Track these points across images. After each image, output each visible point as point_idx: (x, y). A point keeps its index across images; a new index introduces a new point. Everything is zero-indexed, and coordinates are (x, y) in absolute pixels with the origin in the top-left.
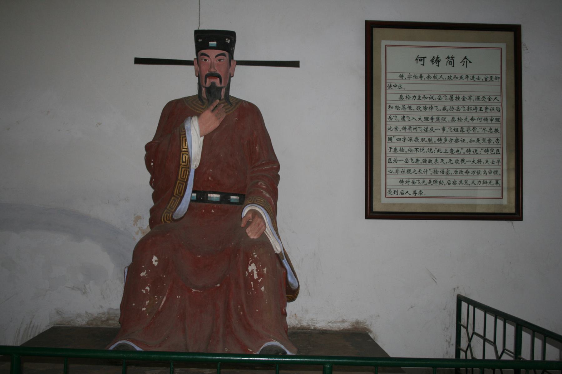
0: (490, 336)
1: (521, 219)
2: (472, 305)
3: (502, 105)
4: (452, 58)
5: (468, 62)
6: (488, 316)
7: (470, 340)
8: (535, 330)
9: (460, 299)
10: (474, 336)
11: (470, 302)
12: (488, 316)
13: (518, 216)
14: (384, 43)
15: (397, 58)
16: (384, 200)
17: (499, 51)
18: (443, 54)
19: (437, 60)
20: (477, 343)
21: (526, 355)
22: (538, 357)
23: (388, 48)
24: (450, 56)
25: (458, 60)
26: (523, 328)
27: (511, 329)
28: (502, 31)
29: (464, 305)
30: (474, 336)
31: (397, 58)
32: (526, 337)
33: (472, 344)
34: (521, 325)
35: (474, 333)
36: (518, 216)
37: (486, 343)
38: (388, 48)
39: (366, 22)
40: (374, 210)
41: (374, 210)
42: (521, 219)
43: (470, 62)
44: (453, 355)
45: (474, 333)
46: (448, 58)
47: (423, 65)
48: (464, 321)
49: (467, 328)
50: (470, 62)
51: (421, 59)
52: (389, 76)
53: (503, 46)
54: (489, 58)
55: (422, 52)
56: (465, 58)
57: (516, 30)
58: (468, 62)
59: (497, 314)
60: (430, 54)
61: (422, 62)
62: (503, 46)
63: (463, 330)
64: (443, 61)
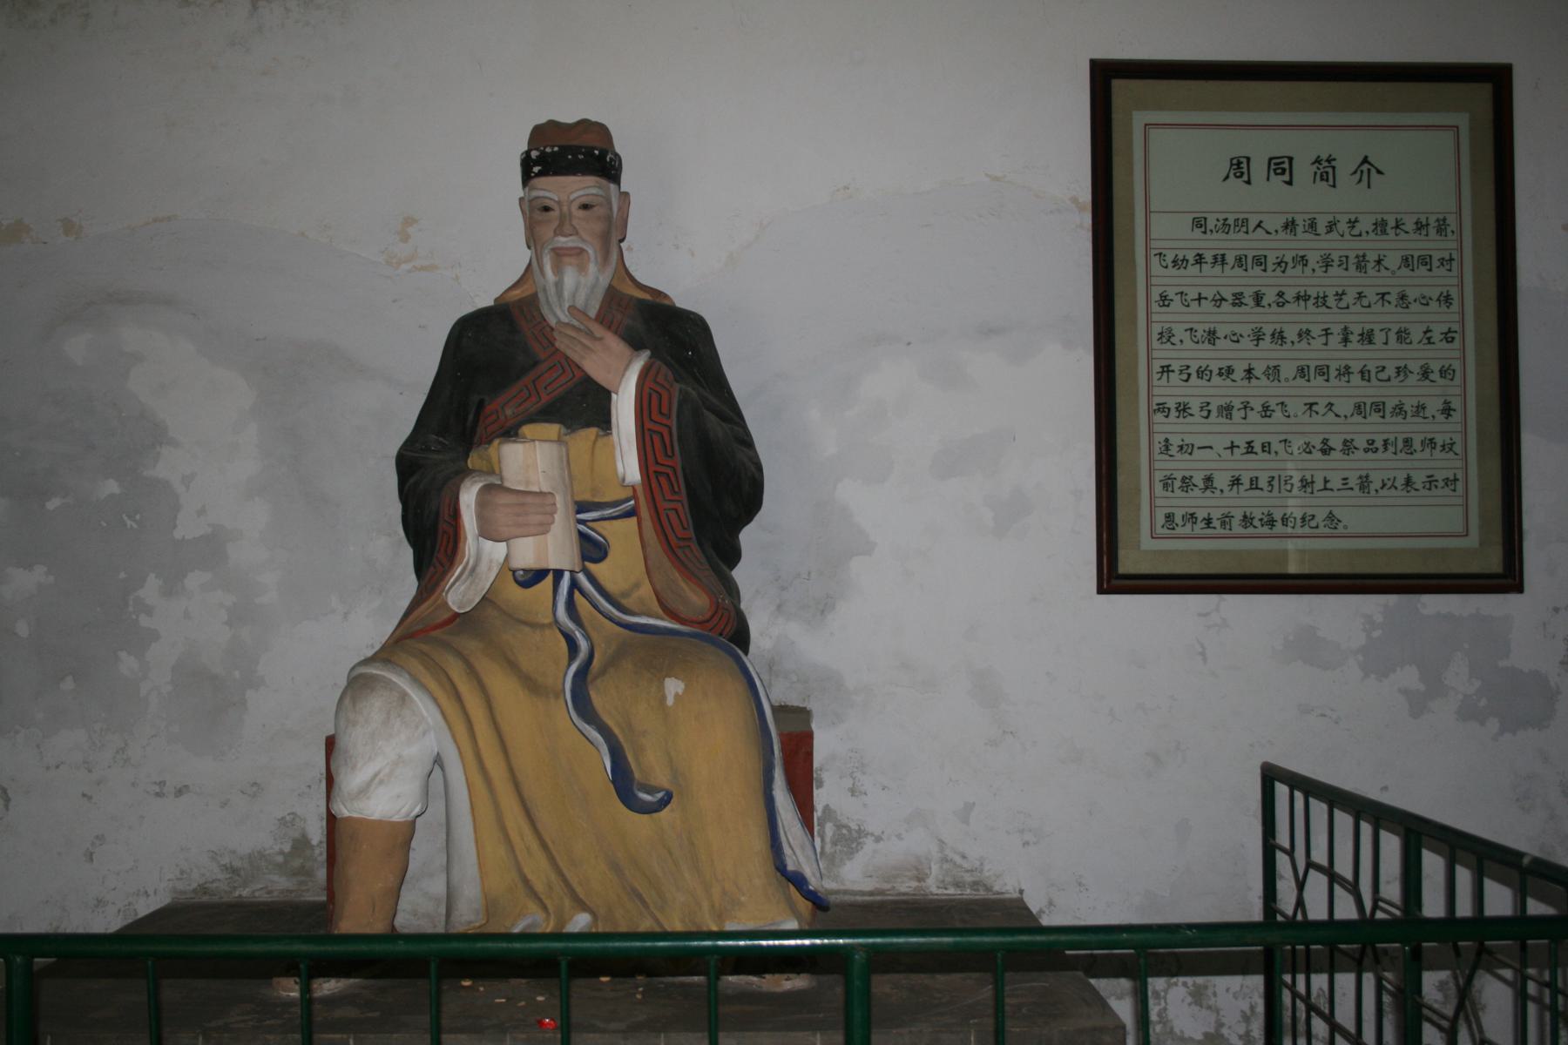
0: (1344, 868)
1: (1519, 589)
2: (1320, 798)
3: (1461, 285)
4: (1329, 161)
5: (1373, 171)
6: (1338, 813)
7: (1301, 885)
8: (1456, 845)
9: (1270, 776)
10: (1312, 872)
11: (1298, 782)
12: (1338, 813)
13: (1510, 581)
14: (1140, 118)
15: (1179, 162)
16: (1147, 543)
17: (1450, 135)
18: (1304, 148)
19: (1281, 167)
20: (1317, 885)
21: (1433, 906)
22: (1464, 909)
23: (1153, 133)
24: (1324, 157)
25: (1345, 167)
26: (1425, 839)
27: (1391, 845)
28: (1439, 81)
29: (1282, 790)
30: (1312, 872)
31: (1179, 162)
32: (1432, 864)
33: (1306, 895)
34: (1417, 833)
35: (1310, 865)
36: (1510, 581)
37: (1337, 887)
38: (1153, 133)
39: (1101, 591)
40: (1122, 570)
41: (1122, 570)
42: (1519, 589)
43: (1379, 172)
44: (1257, 915)
45: (1310, 865)
46: (1318, 161)
47: (1290, 183)
48: (1283, 839)
49: (1290, 853)
50: (1379, 172)
51: (1239, 168)
52: (1160, 226)
53: (1462, 120)
54: (1421, 162)
55: (1239, 144)
56: (1365, 160)
57: (1498, 79)
58: (1373, 171)
59: (1336, 798)
60: (1259, 148)
61: (1286, 177)
62: (1462, 120)
63: (1282, 860)
64: (1303, 171)
